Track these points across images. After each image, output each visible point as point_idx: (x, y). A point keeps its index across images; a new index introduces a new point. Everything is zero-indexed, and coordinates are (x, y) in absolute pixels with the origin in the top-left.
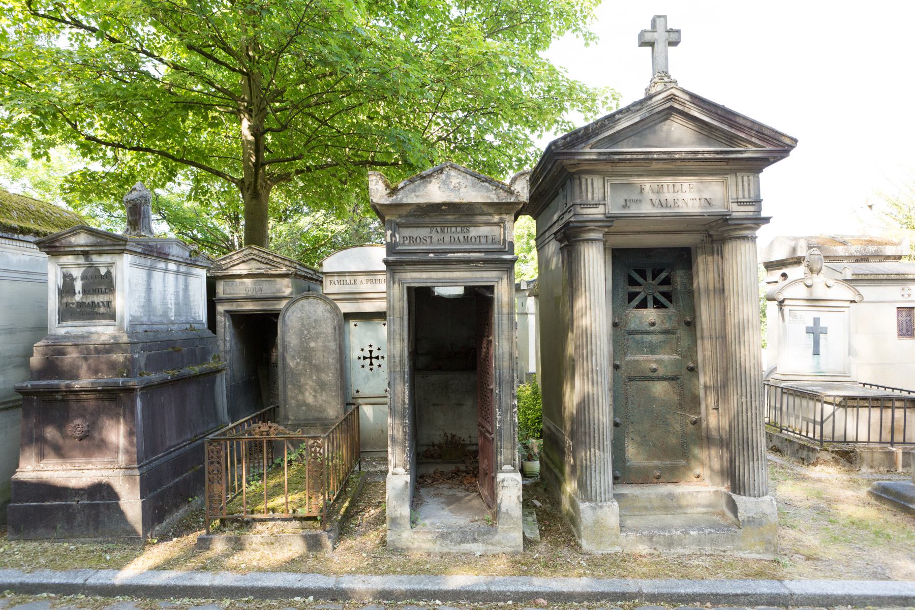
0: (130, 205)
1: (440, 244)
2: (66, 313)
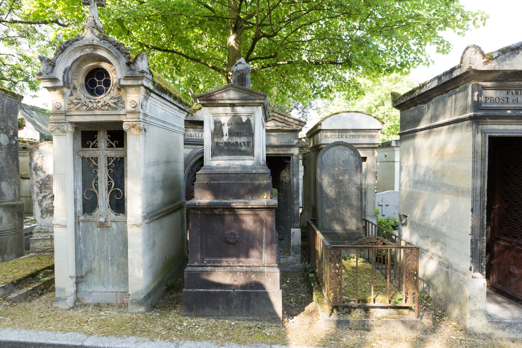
0: (239, 74)
1: (514, 103)
2: (218, 150)
